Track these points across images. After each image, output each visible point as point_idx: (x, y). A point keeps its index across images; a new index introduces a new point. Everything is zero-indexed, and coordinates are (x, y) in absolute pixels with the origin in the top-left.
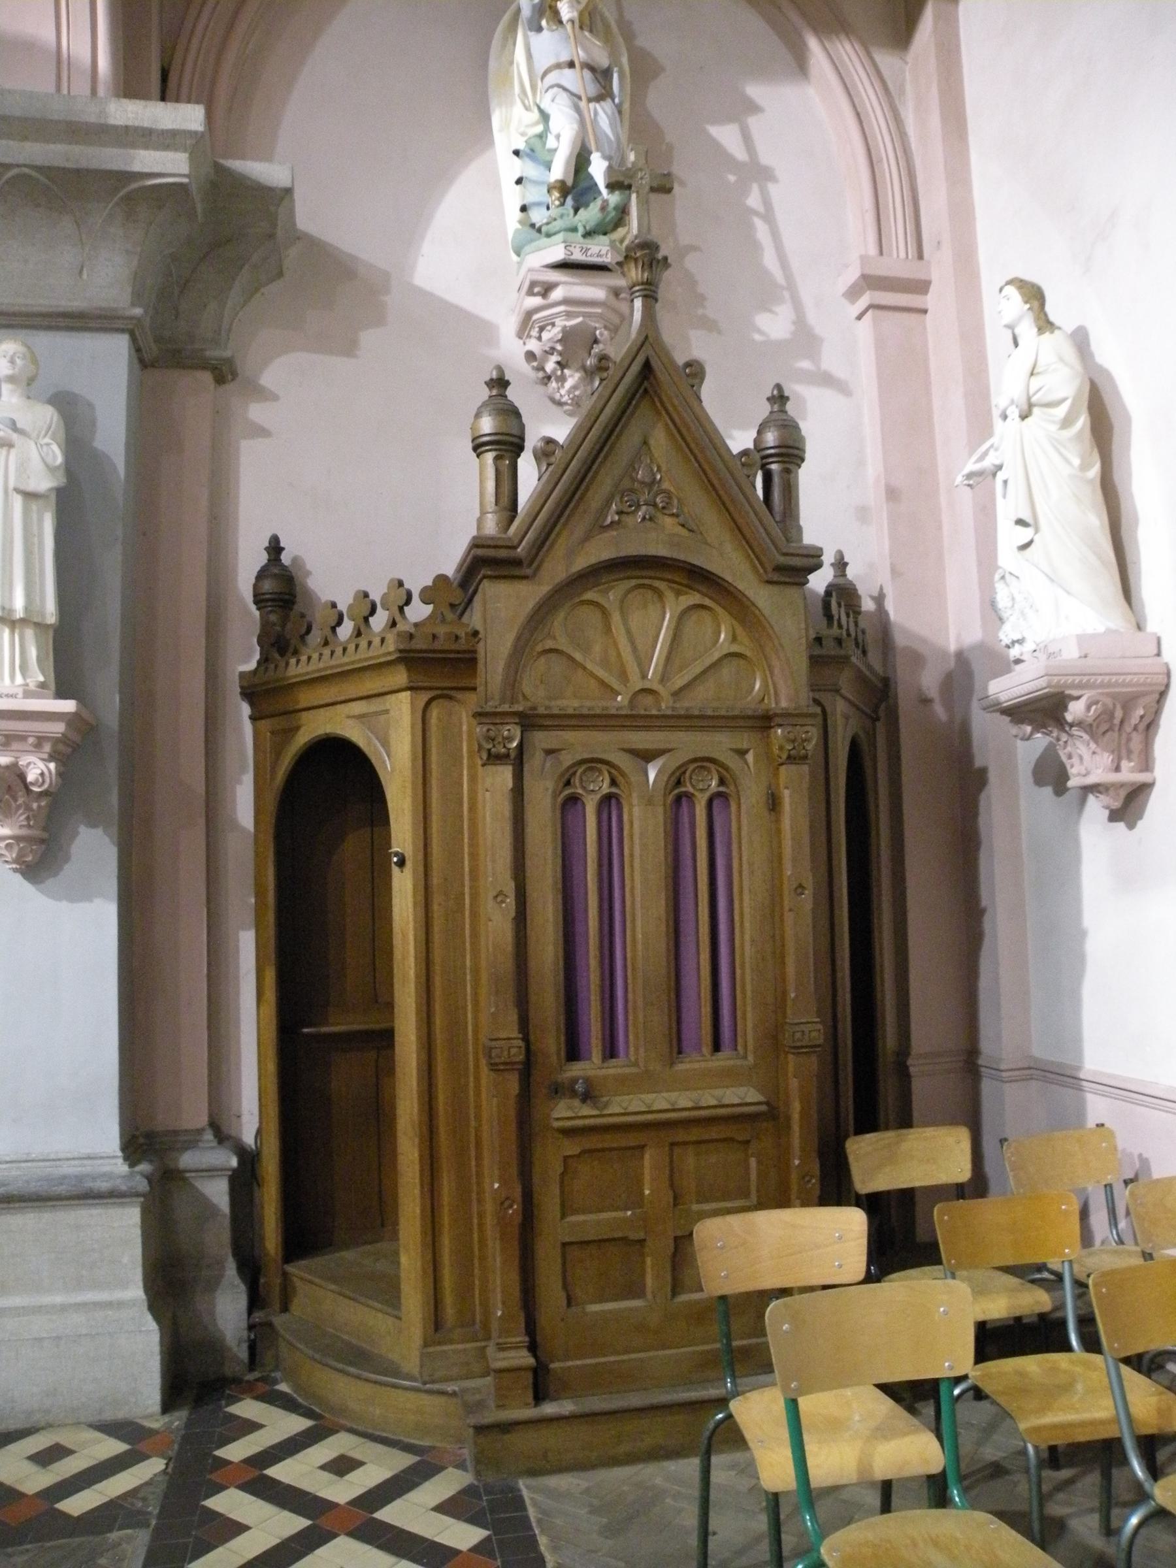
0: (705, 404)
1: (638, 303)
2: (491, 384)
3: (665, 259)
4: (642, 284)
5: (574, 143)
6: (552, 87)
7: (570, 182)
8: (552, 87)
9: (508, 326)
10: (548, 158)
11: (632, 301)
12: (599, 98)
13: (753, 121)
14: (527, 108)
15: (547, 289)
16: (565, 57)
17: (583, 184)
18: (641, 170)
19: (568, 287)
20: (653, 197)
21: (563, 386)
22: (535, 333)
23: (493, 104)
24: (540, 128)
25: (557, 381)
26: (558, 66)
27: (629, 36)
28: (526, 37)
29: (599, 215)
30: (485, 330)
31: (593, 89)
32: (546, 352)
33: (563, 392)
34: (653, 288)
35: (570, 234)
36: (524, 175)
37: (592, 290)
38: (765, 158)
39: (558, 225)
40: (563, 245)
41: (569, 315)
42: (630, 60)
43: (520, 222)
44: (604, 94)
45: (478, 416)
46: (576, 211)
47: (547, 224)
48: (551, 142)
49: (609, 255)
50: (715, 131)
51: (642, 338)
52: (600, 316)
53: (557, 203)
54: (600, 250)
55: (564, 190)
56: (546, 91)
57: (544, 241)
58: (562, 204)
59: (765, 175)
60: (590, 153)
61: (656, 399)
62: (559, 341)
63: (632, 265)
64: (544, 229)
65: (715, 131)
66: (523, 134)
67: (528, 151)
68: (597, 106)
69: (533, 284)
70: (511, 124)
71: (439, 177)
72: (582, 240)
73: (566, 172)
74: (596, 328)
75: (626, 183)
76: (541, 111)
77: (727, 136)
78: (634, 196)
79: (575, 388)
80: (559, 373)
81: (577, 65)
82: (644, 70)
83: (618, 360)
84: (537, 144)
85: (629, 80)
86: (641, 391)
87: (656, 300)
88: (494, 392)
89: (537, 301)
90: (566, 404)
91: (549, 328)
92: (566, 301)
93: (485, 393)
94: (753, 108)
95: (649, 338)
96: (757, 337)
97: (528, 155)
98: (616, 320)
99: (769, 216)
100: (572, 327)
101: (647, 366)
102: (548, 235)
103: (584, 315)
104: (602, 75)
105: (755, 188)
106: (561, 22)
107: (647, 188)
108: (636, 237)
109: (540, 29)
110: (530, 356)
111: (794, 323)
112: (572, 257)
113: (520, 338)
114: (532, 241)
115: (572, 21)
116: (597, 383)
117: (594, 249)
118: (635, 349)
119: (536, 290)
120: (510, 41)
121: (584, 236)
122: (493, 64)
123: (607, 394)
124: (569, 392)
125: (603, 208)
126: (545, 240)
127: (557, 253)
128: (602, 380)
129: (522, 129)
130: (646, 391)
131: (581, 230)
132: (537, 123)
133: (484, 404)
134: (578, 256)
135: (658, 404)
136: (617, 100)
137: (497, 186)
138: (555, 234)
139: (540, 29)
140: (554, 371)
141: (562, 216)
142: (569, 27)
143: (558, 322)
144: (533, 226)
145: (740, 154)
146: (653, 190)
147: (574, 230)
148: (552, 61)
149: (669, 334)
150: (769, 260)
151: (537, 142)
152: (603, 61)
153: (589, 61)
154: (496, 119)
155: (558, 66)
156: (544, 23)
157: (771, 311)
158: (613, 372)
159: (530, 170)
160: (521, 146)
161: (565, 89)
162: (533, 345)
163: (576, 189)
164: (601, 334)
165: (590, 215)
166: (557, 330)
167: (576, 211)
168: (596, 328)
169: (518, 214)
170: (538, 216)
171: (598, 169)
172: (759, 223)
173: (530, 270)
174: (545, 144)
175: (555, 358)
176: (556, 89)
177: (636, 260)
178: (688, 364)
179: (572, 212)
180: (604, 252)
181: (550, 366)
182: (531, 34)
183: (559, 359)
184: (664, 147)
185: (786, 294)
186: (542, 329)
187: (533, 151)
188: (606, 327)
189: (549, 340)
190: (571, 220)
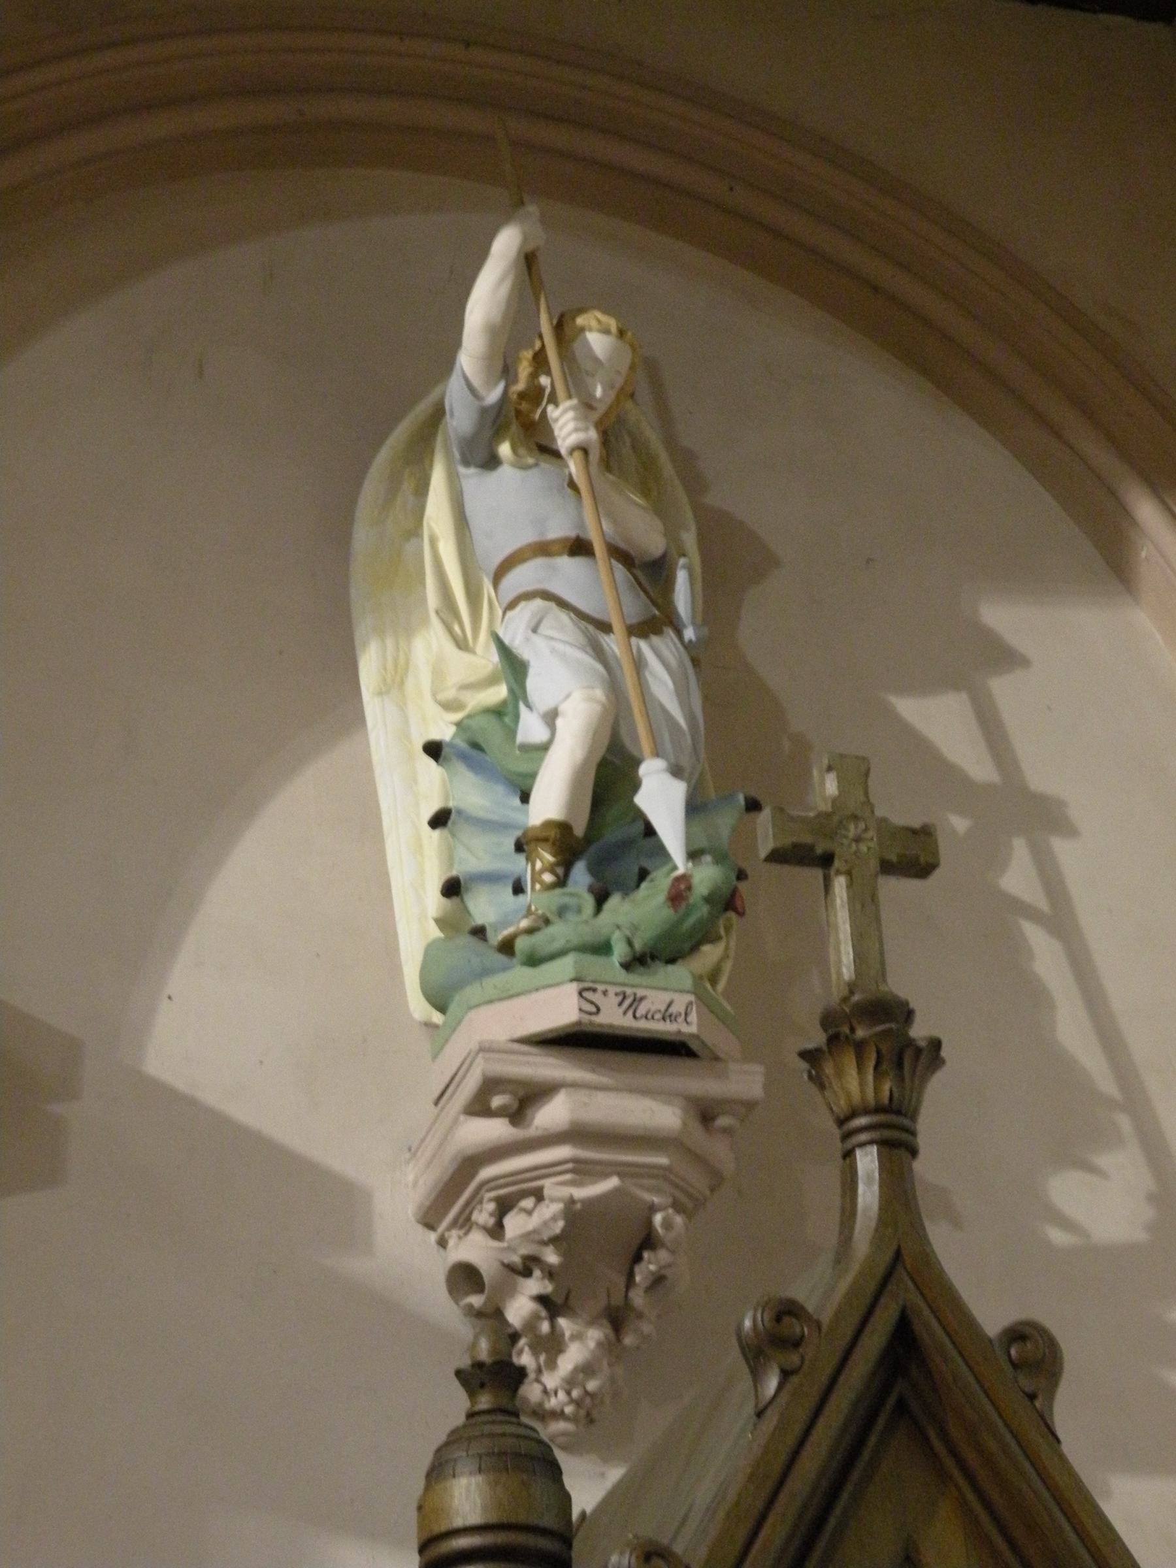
0: (1066, 1448)
1: (867, 1161)
2: (472, 1378)
3: (936, 1045)
4: (878, 1109)
5: (596, 733)
6: (528, 596)
7: (579, 830)
8: (528, 596)
9: (397, 1194)
10: (523, 767)
11: (849, 1154)
12: (645, 628)
13: (1003, 689)
14: (462, 644)
15: (528, 1097)
16: (559, 528)
17: (612, 834)
18: (855, 818)
19: (582, 1096)
20: (893, 888)
21: (552, 1364)
22: (484, 1215)
23: (361, 630)
24: (500, 692)
25: (535, 1349)
26: (543, 549)
27: (695, 484)
28: (453, 481)
29: (668, 913)
30: (335, 1205)
31: (635, 607)
32: (510, 1268)
33: (551, 1380)
34: (906, 1122)
35: (589, 959)
36: (451, 804)
37: (646, 1106)
38: (1040, 777)
39: (559, 933)
40: (574, 987)
41: (582, 1171)
42: (701, 538)
43: (441, 922)
44: (655, 621)
45: (439, 1470)
46: (601, 899)
47: (530, 931)
48: (531, 728)
49: (693, 1017)
50: (908, 708)
51: (887, 1256)
52: (664, 1173)
53: (548, 878)
54: (665, 1002)
55: (566, 845)
56: (511, 605)
57: (520, 974)
58: (561, 882)
59: (1044, 817)
60: (636, 762)
61: (932, 1434)
62: (555, 1241)
63: (849, 1062)
64: (521, 944)
65: (908, 708)
66: (449, 706)
67: (463, 745)
68: (643, 645)
69: (490, 1085)
70: (415, 680)
71: (217, 799)
72: (622, 975)
73: (572, 803)
74: (652, 1209)
75: (819, 851)
76: (505, 651)
77: (940, 720)
78: (840, 884)
79: (586, 1370)
80: (545, 1327)
81: (599, 548)
82: (735, 561)
83: (826, 1318)
84: (492, 734)
85: (699, 579)
86: (891, 1401)
87: (913, 1152)
88: (485, 1401)
89: (495, 1130)
90: (558, 1415)
91: (528, 1203)
92: (575, 1134)
93: (455, 1405)
94: (1005, 658)
95: (904, 1262)
96: (1058, 1236)
97: (464, 757)
98: (698, 1181)
99: (1061, 921)
100: (589, 1203)
101: (904, 1334)
102: (534, 960)
103: (622, 1170)
104: (651, 574)
105: (1020, 848)
106: (556, 454)
107: (874, 864)
108: (852, 988)
109: (491, 462)
110: (465, 1277)
111: (1152, 1198)
112: (600, 1019)
113: (431, 1227)
114: (486, 972)
115: (583, 449)
116: (772, 1384)
117: (655, 1000)
118: (872, 1286)
119: (497, 1101)
120: (408, 486)
121: (627, 966)
122: (363, 536)
123: (802, 1415)
124: (570, 1383)
125: (679, 894)
126: (527, 971)
127: (559, 1008)
128: (786, 1374)
129: (450, 694)
130: (901, 1406)
131: (620, 951)
132: (491, 681)
133: (455, 1438)
134: (613, 1017)
135: (937, 1444)
136: (689, 634)
137: (367, 824)
138: (552, 957)
139: (491, 462)
140: (531, 1324)
141: (562, 911)
142: (574, 466)
143: (549, 1186)
144: (479, 932)
145: (978, 767)
146: (887, 868)
147: (602, 948)
148: (526, 537)
149: (955, 1252)
150: (1072, 1030)
151: (490, 725)
152: (653, 542)
153: (622, 545)
154: (370, 667)
155: (543, 549)
156: (505, 449)
157: (1091, 1169)
158: (820, 1356)
159: (473, 794)
160: (444, 731)
161: (562, 604)
162: (474, 1248)
163: (600, 841)
164: (667, 1224)
165: (640, 912)
166: (549, 1210)
167: (601, 899)
168: (652, 1209)
169: (434, 902)
170: (487, 906)
171: (660, 798)
172: (1036, 936)
173: (485, 1049)
174: (512, 733)
175: (535, 1285)
176: (538, 603)
177: (860, 1048)
178: (1018, 1334)
179: (589, 902)
180: (678, 1008)
181: (519, 1309)
182: (471, 477)
183: (548, 1288)
184: (787, 745)
185: (1124, 1122)
186: (505, 1206)
187: (482, 747)
188: (677, 1206)
189: (527, 1236)
190: (724, 939)
